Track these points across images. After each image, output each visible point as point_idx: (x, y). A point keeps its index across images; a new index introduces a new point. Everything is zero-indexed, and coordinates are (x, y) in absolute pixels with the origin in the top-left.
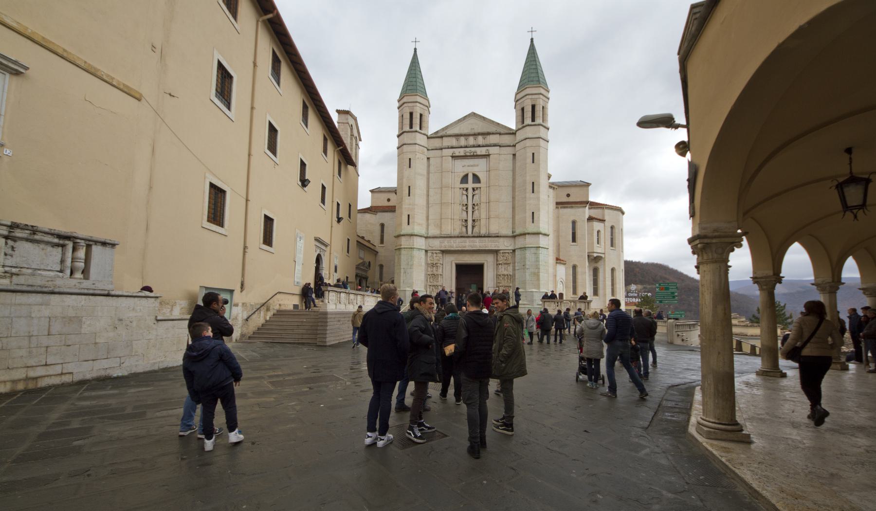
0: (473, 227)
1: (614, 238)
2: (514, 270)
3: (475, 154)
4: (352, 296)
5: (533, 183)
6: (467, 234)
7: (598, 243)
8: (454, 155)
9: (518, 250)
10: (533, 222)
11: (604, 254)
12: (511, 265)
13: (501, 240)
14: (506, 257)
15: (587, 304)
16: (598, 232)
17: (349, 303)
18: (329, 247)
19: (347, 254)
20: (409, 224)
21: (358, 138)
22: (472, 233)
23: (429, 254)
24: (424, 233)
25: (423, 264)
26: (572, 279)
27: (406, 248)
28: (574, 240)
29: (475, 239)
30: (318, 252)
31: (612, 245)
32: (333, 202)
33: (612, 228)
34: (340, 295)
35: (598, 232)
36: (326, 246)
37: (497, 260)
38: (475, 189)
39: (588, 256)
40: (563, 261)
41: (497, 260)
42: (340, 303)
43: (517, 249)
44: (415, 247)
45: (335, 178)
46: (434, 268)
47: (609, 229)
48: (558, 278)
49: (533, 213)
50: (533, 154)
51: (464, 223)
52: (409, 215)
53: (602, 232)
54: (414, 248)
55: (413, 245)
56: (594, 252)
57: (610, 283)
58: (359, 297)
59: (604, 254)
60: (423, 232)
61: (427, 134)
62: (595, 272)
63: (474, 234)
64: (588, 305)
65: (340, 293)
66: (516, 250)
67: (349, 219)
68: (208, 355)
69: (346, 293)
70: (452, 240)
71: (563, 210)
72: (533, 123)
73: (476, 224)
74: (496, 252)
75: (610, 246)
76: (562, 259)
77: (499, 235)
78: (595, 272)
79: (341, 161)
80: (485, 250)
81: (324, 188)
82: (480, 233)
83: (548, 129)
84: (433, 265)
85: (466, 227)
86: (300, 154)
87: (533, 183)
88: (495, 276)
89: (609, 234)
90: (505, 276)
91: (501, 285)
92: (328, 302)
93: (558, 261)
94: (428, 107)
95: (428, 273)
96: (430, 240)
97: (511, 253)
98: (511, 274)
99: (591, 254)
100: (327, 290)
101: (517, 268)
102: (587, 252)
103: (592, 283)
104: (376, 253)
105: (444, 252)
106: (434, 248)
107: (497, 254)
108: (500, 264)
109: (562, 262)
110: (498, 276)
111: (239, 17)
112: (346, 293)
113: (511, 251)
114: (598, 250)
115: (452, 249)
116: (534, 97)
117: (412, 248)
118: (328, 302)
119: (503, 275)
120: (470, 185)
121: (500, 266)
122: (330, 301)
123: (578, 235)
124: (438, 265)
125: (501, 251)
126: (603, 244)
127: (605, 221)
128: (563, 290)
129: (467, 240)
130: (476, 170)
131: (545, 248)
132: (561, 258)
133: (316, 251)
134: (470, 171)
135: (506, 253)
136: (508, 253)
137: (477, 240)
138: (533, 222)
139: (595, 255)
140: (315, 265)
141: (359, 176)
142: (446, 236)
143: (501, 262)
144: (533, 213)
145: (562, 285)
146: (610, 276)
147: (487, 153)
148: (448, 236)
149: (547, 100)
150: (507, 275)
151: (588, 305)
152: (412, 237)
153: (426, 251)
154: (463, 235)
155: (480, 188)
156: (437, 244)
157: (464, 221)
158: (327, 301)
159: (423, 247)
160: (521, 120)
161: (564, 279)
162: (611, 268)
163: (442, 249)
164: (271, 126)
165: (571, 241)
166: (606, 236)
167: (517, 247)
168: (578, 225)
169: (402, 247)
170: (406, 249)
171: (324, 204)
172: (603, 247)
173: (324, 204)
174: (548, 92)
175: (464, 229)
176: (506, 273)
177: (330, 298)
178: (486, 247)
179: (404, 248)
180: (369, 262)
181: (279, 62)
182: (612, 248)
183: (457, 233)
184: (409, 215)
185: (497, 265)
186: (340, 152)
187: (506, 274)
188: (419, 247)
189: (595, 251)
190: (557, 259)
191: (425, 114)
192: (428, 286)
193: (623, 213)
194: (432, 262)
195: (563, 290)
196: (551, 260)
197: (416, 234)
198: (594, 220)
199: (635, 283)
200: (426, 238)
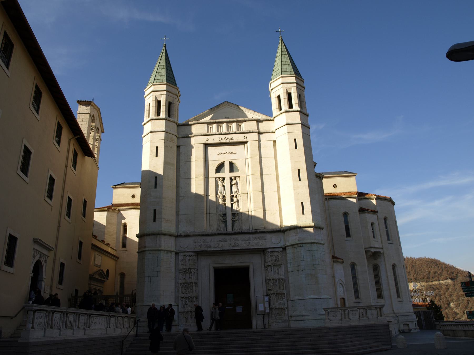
0: (233, 222)
1: (389, 230)
2: (287, 272)
3: (231, 141)
4: (71, 318)
5: (299, 170)
6: (226, 230)
7: (374, 237)
8: (208, 142)
9: (290, 247)
10: (303, 213)
11: (382, 248)
12: (283, 266)
13: (268, 236)
14: (276, 257)
15: (378, 310)
16: (372, 224)
17: (66, 327)
18: (53, 252)
19: (78, 260)
20: (154, 221)
21: (100, 129)
22: (233, 230)
23: (181, 257)
24: (174, 232)
25: (173, 270)
26: (352, 280)
27: (152, 250)
28: (348, 234)
29: (236, 236)
30: (37, 258)
31: (388, 239)
32: (63, 196)
33: (385, 219)
34: (52, 316)
35: (372, 224)
36: (49, 249)
37: (265, 262)
38: (233, 178)
39: (366, 251)
40: (339, 258)
41: (265, 262)
42: (51, 327)
43: (288, 246)
44: (162, 248)
45: (69, 169)
46: (187, 275)
47: (383, 221)
48: (337, 280)
49: (302, 203)
50: (295, 140)
51: (221, 218)
52: (155, 211)
53: (376, 224)
54: (161, 250)
55: (160, 246)
56: (371, 248)
57: (394, 283)
58: (82, 318)
59: (382, 248)
60: (172, 230)
61: (176, 121)
62: (376, 268)
63: (236, 230)
64: (380, 310)
65: (53, 313)
66: (287, 248)
67: (82, 217)
68: (85, 320)
69: (61, 312)
70: (209, 238)
71: (332, 201)
72: (291, 110)
73: (237, 218)
74: (262, 251)
75: (387, 240)
76: (338, 257)
77: (265, 230)
78: (376, 268)
79: (62, 125)
80: (250, 249)
81: (52, 180)
82: (242, 229)
83: (308, 116)
84: (186, 271)
85: (225, 222)
86: (24, 140)
87: (299, 170)
88: (264, 281)
89: (384, 226)
90: (276, 281)
91: (272, 292)
92: (33, 328)
93: (335, 260)
94: (177, 96)
95: (180, 281)
96: (182, 239)
97: (281, 251)
98: (284, 277)
99: (368, 249)
100: (32, 310)
101: (290, 270)
102: (364, 248)
103: (374, 283)
104: (116, 259)
105: (200, 254)
106: (186, 250)
107: (265, 254)
108: (268, 266)
109: (339, 260)
110: (267, 280)
111: (76, 170)
112: (61, 312)
113: (281, 249)
114: (376, 244)
115: (209, 249)
116: (289, 85)
117: (158, 250)
118: (33, 328)
119: (273, 279)
120: (226, 173)
121: (269, 269)
122: (35, 326)
123: (352, 229)
124: (192, 270)
125: (270, 250)
126: (380, 237)
127: (377, 212)
128: (344, 295)
129: (227, 237)
130: (232, 158)
131: (321, 244)
132: (336, 255)
133: (34, 257)
134: (227, 159)
135: (275, 251)
136: (278, 251)
137: (240, 237)
138: (303, 213)
139: (373, 250)
140: (32, 275)
141: (99, 169)
142: (201, 233)
143: (270, 264)
144: (302, 203)
145: (342, 289)
146: (392, 274)
147: (245, 140)
148: (203, 233)
149: (303, 89)
150: (279, 279)
151: (380, 310)
152: (158, 236)
153: (177, 253)
154: (221, 232)
155: (239, 177)
156: (189, 244)
157: (222, 215)
158: (31, 325)
159: (173, 249)
160: (278, 107)
161: (344, 281)
162: (392, 265)
163: (196, 250)
164: (26, 149)
165: (346, 236)
166: (380, 228)
167: (287, 244)
168: (350, 217)
169: (147, 249)
170: (151, 252)
171: (51, 199)
172: (380, 241)
173: (51, 199)
174: (303, 82)
175: (222, 226)
176: (276, 276)
177: (36, 321)
178: (251, 246)
179: (149, 250)
180: (108, 271)
181: (12, 45)
182: (389, 242)
183: (214, 229)
184: (155, 211)
185: (265, 267)
186: (76, 140)
187: (277, 278)
188: (168, 249)
189: (372, 246)
190: (334, 257)
191: (176, 102)
192: (180, 298)
193: (393, 204)
194: (184, 267)
195: (344, 295)
196: (328, 259)
197: (163, 232)
198: (366, 211)
199: (416, 280)
200: (177, 237)
